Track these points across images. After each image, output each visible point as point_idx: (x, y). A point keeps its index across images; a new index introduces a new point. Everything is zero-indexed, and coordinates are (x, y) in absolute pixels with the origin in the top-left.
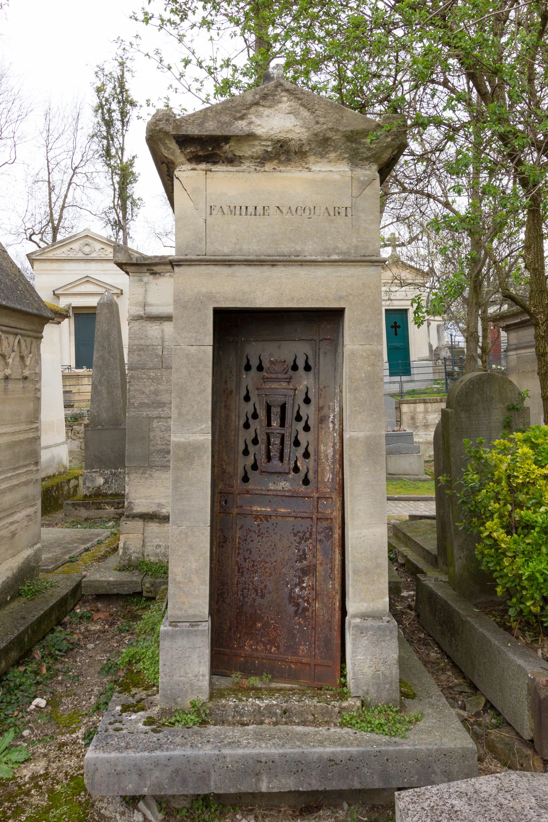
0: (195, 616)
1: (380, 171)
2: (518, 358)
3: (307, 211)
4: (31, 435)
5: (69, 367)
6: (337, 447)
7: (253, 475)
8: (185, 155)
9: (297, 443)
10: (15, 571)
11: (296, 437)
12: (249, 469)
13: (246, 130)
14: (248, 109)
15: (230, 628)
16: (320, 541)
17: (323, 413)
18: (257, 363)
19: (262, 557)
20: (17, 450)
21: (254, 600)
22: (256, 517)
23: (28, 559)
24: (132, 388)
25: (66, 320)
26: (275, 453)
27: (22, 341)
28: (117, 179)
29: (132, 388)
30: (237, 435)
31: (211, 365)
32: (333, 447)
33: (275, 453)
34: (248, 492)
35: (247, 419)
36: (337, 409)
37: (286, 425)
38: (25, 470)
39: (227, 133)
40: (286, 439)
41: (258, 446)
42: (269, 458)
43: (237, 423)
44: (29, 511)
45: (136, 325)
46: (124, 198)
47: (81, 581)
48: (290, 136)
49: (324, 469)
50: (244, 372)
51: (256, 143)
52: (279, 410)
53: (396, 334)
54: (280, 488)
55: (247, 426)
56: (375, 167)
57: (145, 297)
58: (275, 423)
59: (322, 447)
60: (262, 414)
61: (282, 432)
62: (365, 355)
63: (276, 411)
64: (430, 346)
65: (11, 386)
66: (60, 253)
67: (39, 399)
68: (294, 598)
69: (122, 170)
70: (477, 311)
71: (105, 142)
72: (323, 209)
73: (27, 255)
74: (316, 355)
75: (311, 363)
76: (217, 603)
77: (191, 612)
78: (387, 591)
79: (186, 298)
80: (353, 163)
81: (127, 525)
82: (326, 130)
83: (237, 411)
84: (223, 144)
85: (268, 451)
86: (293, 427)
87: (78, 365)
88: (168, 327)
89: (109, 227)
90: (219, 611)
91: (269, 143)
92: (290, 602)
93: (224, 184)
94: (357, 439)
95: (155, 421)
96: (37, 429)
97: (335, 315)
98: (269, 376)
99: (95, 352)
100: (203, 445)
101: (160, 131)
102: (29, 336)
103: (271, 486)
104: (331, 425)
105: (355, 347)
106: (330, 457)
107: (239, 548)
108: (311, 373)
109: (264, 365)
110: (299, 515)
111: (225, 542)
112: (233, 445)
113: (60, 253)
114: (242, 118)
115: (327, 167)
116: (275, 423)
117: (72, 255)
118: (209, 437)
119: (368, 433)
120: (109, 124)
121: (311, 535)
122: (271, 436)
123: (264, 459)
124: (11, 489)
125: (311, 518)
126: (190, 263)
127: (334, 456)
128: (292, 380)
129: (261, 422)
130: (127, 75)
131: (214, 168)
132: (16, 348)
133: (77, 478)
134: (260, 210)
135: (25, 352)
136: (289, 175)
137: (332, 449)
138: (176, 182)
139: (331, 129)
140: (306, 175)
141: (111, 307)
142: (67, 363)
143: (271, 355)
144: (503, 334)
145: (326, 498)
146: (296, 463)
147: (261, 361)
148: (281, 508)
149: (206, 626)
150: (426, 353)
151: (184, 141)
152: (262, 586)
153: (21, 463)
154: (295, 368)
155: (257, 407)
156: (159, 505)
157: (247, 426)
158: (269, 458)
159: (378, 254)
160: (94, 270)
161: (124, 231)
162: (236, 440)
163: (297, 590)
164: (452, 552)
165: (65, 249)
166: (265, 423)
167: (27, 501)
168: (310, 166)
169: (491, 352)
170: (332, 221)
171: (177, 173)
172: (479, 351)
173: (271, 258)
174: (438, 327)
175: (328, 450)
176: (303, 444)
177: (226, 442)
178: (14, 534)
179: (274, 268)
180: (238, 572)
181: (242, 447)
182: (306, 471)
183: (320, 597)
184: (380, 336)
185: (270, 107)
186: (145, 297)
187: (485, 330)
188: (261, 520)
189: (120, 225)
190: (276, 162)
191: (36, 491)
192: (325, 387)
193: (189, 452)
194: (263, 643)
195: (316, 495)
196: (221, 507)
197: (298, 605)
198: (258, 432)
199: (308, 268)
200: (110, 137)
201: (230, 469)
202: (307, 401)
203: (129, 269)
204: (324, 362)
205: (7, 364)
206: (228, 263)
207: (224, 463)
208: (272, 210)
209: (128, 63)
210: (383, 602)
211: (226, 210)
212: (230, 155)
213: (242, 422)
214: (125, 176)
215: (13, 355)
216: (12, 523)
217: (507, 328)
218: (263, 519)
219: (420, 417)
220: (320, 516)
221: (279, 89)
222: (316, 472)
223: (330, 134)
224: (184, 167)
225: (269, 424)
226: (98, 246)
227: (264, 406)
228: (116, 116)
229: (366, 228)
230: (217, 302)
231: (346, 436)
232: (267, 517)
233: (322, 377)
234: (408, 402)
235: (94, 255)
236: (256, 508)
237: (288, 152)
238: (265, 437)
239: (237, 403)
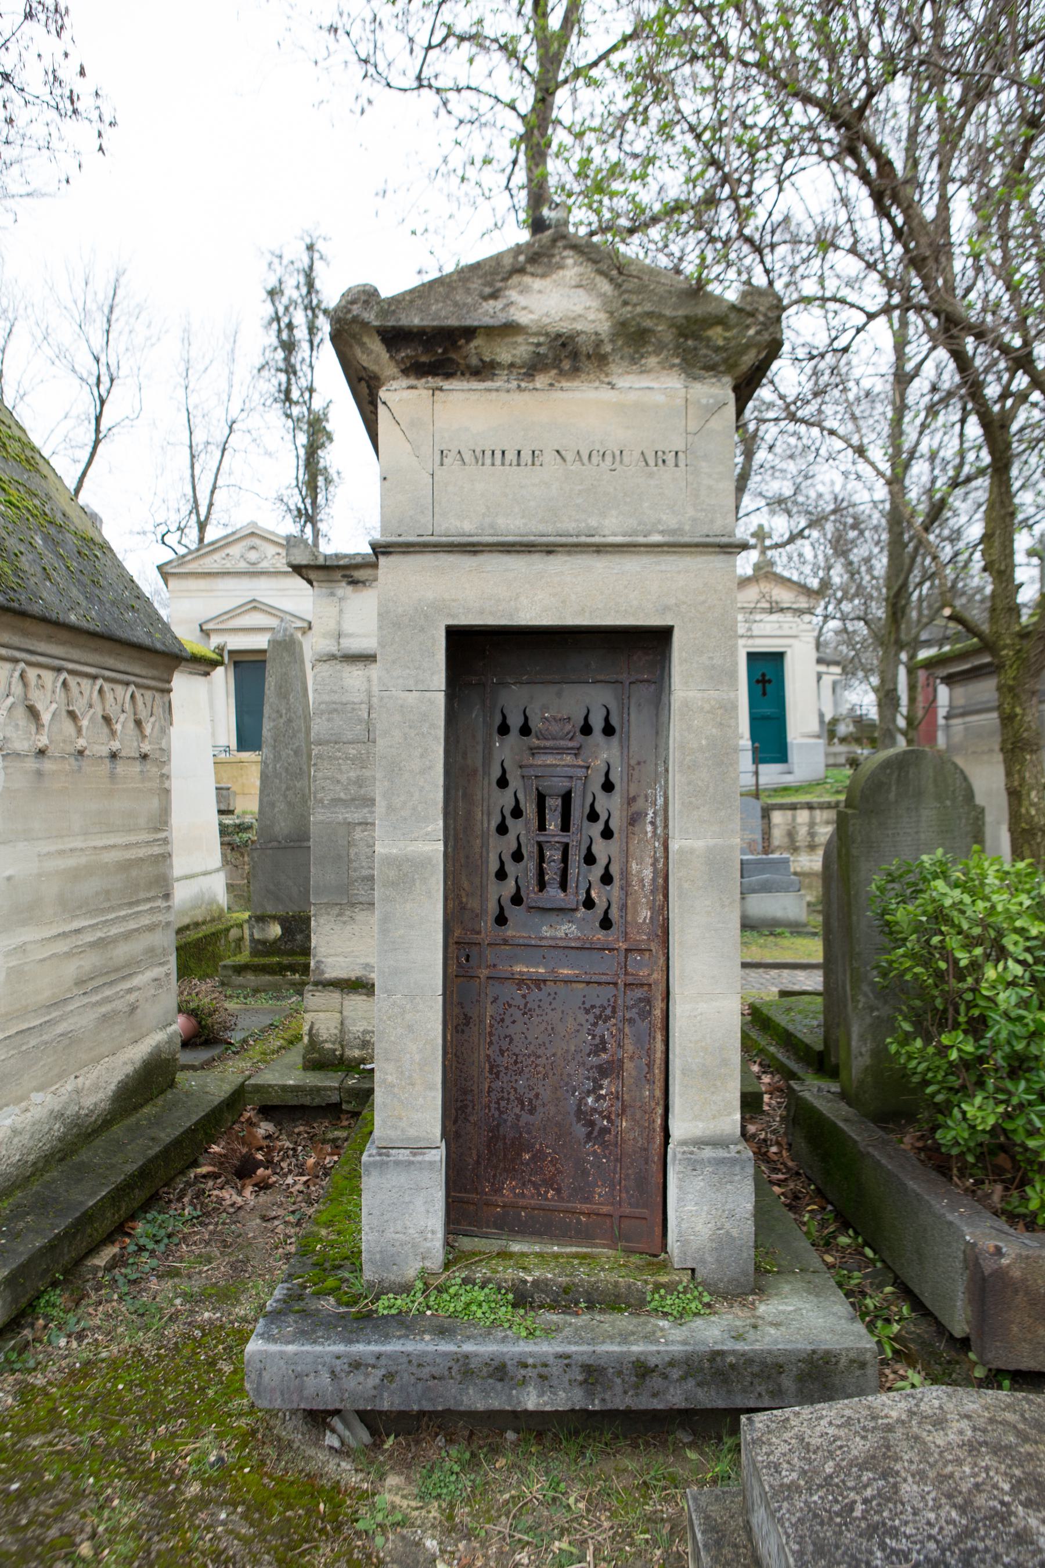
0: (418, 1139)
1: (736, 389)
2: (966, 729)
3: (609, 458)
4: (157, 850)
5: (227, 749)
6: (660, 865)
7: (513, 913)
8: (397, 362)
9: (590, 859)
10: (137, 1065)
11: (589, 849)
12: (506, 903)
13: (502, 319)
14: (505, 280)
15: (478, 1163)
16: (631, 1021)
17: (635, 808)
18: (520, 721)
19: (532, 1048)
20: (134, 873)
21: (518, 1117)
22: (521, 982)
23: (157, 1046)
24: (321, 773)
25: (220, 670)
26: (552, 872)
27: (138, 695)
28: (302, 439)
29: (320, 775)
30: (485, 845)
31: (441, 723)
32: (654, 865)
33: (552, 872)
34: (505, 942)
35: (504, 817)
36: (660, 801)
37: (573, 829)
38: (148, 906)
39: (468, 322)
40: (571, 851)
41: (523, 864)
42: (542, 885)
44: (157, 972)
45: (325, 669)
46: (313, 474)
47: (243, 1085)
48: (579, 327)
49: (636, 903)
50: (496, 737)
51: (520, 339)
52: (559, 801)
53: (764, 694)
54: (560, 934)
55: (502, 829)
56: (728, 381)
57: (339, 623)
58: (553, 825)
60: (530, 809)
62: (707, 707)
63: (554, 803)
64: (821, 716)
65: (121, 768)
66: (214, 562)
67: (167, 791)
68: (585, 1113)
69: (310, 424)
70: (897, 655)
71: (283, 377)
72: (637, 455)
73: (159, 568)
74: (624, 708)
75: (614, 721)
76: (455, 1122)
77: (412, 1132)
78: (737, 1103)
79: (400, 610)
80: (688, 375)
81: (315, 999)
82: (640, 315)
84: (462, 342)
85: (541, 873)
87: (242, 746)
88: (374, 671)
89: (289, 519)
90: (457, 1135)
91: (542, 339)
92: (579, 1120)
93: (465, 411)
94: (692, 851)
95: (359, 829)
96: (166, 841)
97: (658, 639)
99: (265, 720)
100: (430, 859)
101: (355, 319)
102: (148, 688)
103: (546, 931)
104: (649, 828)
105: (691, 694)
106: (647, 882)
107: (491, 1034)
108: (615, 740)
109: (531, 724)
110: (595, 978)
111: (467, 1024)
113: (214, 562)
114: (494, 296)
115: (644, 381)
116: (553, 825)
117: (229, 565)
118: (440, 846)
119: (711, 842)
120: (289, 347)
121: (614, 1011)
123: (534, 882)
124: (127, 936)
125: (615, 984)
126: (407, 548)
127: (654, 880)
129: (527, 822)
130: (318, 265)
131: (446, 385)
132: (127, 706)
133: (240, 926)
134: (526, 456)
135: (143, 714)
136: (577, 395)
137: (650, 869)
138: (381, 409)
139: (649, 315)
140: (606, 395)
141: (287, 646)
142: (223, 741)
143: (545, 708)
144: (943, 693)
145: (640, 951)
146: (588, 892)
147: (526, 718)
149: (438, 1156)
150: (814, 726)
151: (395, 338)
152: (532, 1095)
153: (142, 895)
154: (587, 729)
155: (521, 796)
156: (367, 966)
157: (502, 829)
158: (542, 885)
159: (732, 534)
160: (265, 590)
161: (314, 525)
163: (590, 1100)
164: (849, 1044)
165: (217, 556)
166: (535, 823)
167: (152, 955)
168: (614, 380)
169: (921, 725)
170: (651, 475)
171: (383, 394)
172: (901, 723)
173: (544, 539)
174: (835, 684)
175: (643, 871)
176: (602, 861)
178: (133, 1009)
179: (551, 557)
180: (491, 1072)
181: (494, 867)
182: (605, 905)
183: (628, 1112)
184: (733, 675)
185: (543, 276)
186: (339, 623)
187: (912, 687)
189: (309, 516)
190: (554, 372)
191: (167, 941)
193: (406, 873)
194: (534, 1184)
195: (623, 946)
196: (460, 965)
197: (591, 1124)
198: (522, 839)
199: (609, 557)
200: (290, 370)
201: (473, 903)
202: (608, 787)
203: (312, 575)
204: (637, 723)
205: (113, 733)
206: (471, 548)
208: (549, 457)
209: (319, 245)
210: (730, 1121)
211: (468, 456)
212: (474, 361)
213: (494, 824)
214: (316, 432)
215: (123, 717)
216: (130, 991)
217: (949, 680)
219: (803, 831)
220: (630, 979)
221: (560, 244)
222: (624, 907)
223: (648, 323)
224: (395, 384)
225: (542, 827)
226: (272, 550)
228: (301, 334)
229: (710, 488)
230: (453, 616)
231: (674, 846)
232: (539, 983)
233: (633, 743)
234: (781, 807)
235: (264, 565)
237: (575, 355)
238: (535, 849)
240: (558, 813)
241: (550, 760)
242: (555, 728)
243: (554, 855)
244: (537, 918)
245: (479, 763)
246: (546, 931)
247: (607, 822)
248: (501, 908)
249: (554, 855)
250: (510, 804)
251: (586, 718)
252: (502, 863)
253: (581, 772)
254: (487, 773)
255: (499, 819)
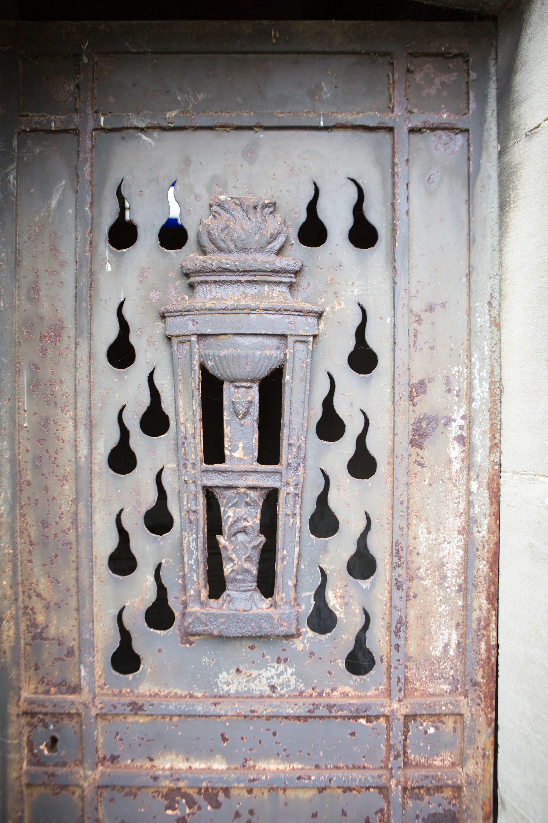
6: (482, 532)
9: (324, 522)
11: (323, 499)
26: (240, 554)
30: (84, 496)
33: (240, 554)
34: (136, 708)
35: (125, 433)
36: (481, 391)
40: (283, 508)
42: (217, 584)
43: (83, 451)
50: (105, 249)
52: (254, 394)
55: (122, 460)
59: (422, 535)
60: (185, 411)
61: (270, 482)
75: (375, 215)
83: (82, 403)
85: (214, 558)
86: (310, 462)
98: (215, 260)
103: (228, 682)
104: (456, 451)
108: (377, 254)
112: (71, 536)
122: (224, 500)
123: (198, 578)
125: (383, 790)
127: (467, 565)
128: (304, 281)
137: (458, 540)
146: (320, 594)
148: (267, 756)
154: (313, 232)
157: (122, 460)
158: (217, 584)
162: (83, 516)
175: (438, 544)
176: (350, 527)
177: (44, 524)
181: (106, 543)
188: (191, 803)
192: (431, 309)
196: (36, 760)
201: (62, 626)
202: (363, 359)
207: (37, 604)
218: (200, 799)
220: (415, 775)
222: (398, 628)
225: (214, 451)
227: (196, 380)
236: (169, 763)
238: (201, 505)
239: (82, 373)
240: (252, 422)
241: (231, 295)
242: (243, 226)
243: (242, 516)
244: (206, 656)
245: (67, 311)
246: (228, 682)
247: (361, 440)
248: (125, 636)
249: (242, 516)
250: (138, 404)
251: (312, 207)
252: (124, 536)
253: (305, 326)
254: (84, 330)
255: (114, 438)
